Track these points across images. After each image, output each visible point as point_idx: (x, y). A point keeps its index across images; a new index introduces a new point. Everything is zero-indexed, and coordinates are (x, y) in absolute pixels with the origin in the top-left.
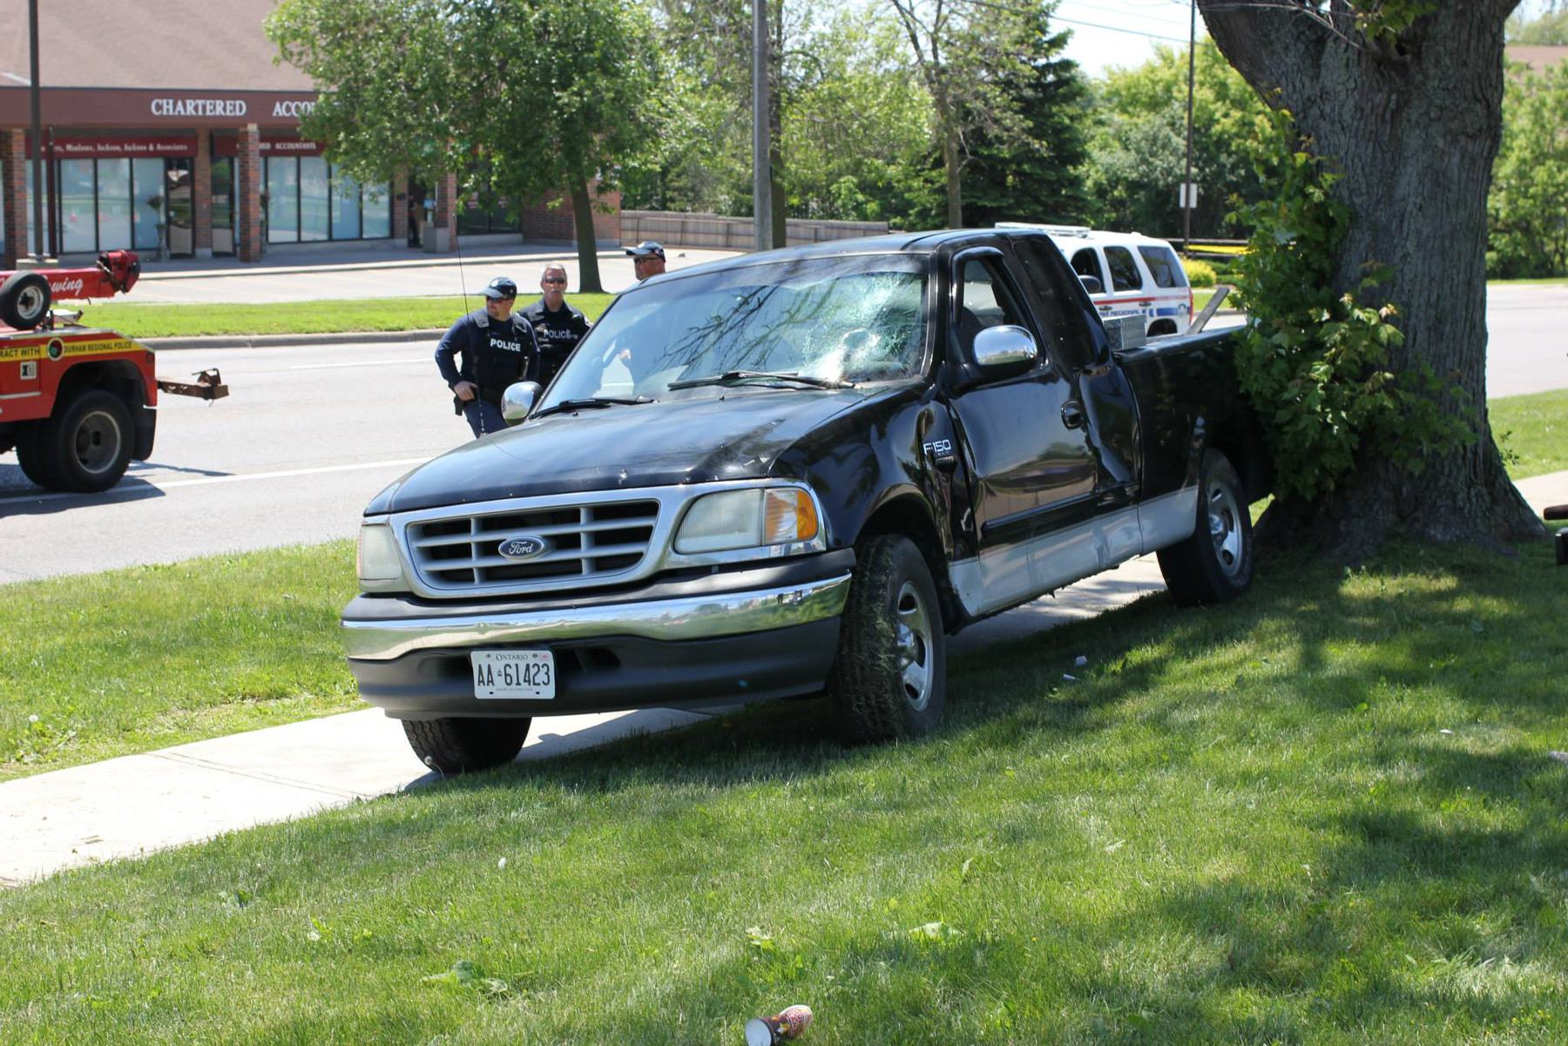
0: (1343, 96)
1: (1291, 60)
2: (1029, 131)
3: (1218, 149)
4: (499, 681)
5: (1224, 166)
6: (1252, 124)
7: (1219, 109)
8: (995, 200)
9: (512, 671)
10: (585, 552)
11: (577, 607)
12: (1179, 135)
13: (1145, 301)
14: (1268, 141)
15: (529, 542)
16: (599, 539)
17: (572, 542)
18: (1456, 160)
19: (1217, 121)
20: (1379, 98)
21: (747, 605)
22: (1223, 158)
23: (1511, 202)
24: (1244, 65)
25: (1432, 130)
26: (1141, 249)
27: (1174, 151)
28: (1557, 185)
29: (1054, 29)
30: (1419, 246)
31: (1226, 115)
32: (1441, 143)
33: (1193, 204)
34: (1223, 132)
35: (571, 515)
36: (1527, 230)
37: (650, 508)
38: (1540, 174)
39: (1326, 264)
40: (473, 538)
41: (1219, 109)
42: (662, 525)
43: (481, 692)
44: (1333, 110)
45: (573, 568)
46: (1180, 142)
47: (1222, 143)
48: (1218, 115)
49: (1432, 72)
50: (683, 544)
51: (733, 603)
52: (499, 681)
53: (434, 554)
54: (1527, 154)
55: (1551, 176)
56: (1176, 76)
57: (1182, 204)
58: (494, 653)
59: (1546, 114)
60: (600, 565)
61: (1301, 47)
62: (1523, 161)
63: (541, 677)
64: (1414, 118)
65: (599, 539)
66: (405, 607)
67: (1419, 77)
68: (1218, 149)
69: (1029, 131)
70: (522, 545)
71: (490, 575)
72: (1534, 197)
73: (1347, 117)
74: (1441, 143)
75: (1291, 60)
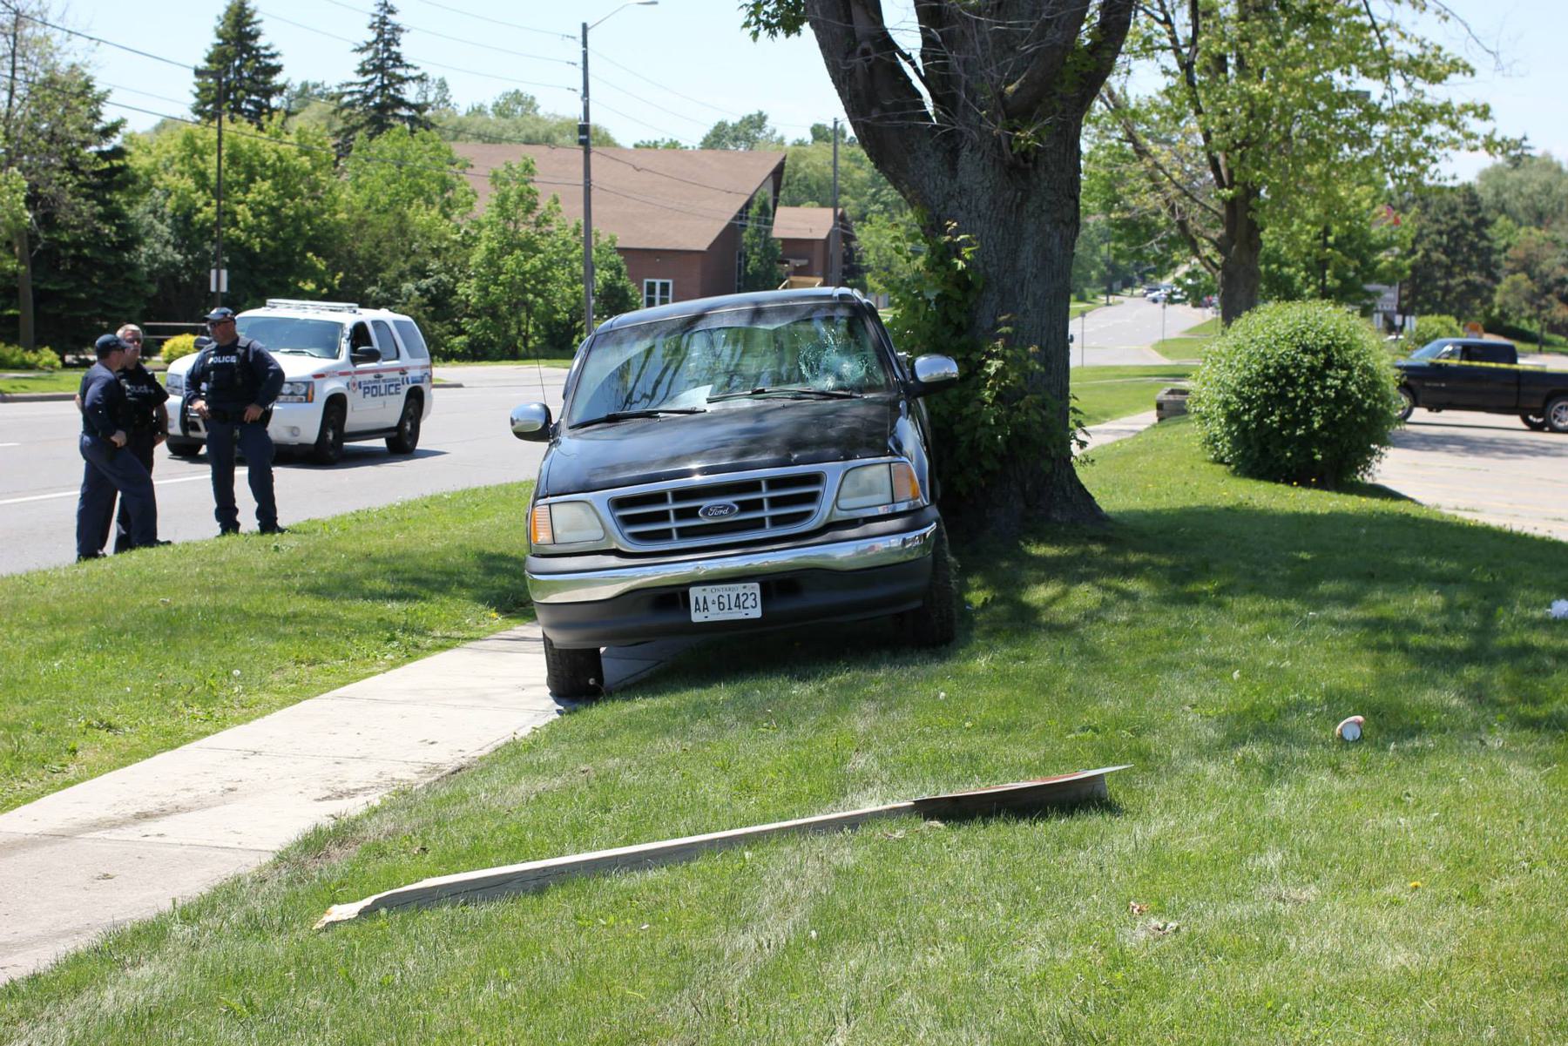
0: (979, 192)
1: (932, 164)
2: (100, 217)
3: (201, 237)
4: (713, 608)
5: (208, 253)
6: (234, 213)
7: (200, 198)
8: (56, 284)
9: (725, 600)
10: (767, 512)
11: (1471, 446)
12: (162, 221)
13: (403, 371)
14: (249, 229)
15: (725, 507)
16: (775, 503)
17: (757, 505)
18: (1057, 240)
19: (200, 210)
20: (1008, 194)
21: (864, 551)
22: (208, 246)
23: (485, 290)
24: (890, 168)
25: (1043, 219)
26: (395, 322)
27: (158, 238)
28: (523, 274)
29: (109, 115)
30: (1035, 304)
31: (208, 204)
32: (1048, 228)
33: (224, 288)
34: (206, 220)
35: (754, 486)
36: (494, 315)
37: (816, 479)
38: (509, 262)
39: (964, 319)
40: (671, 506)
41: (200, 198)
42: (828, 492)
43: (697, 617)
44: (970, 202)
45: (758, 524)
46: (164, 229)
47: (205, 232)
48: (200, 204)
49: (1043, 176)
50: (842, 503)
51: (882, 544)
52: (713, 608)
53: (628, 521)
54: (495, 244)
55: (519, 264)
56: (155, 164)
57: (213, 289)
58: (709, 588)
59: (510, 205)
60: (777, 521)
61: (940, 155)
62: (491, 251)
63: (750, 603)
64: (1031, 209)
65: (775, 503)
66: (613, 561)
67: (1035, 180)
68: (201, 237)
69: (100, 217)
70: (714, 509)
71: (684, 533)
72: (502, 284)
73: (982, 207)
74: (1048, 228)
75: (932, 164)
